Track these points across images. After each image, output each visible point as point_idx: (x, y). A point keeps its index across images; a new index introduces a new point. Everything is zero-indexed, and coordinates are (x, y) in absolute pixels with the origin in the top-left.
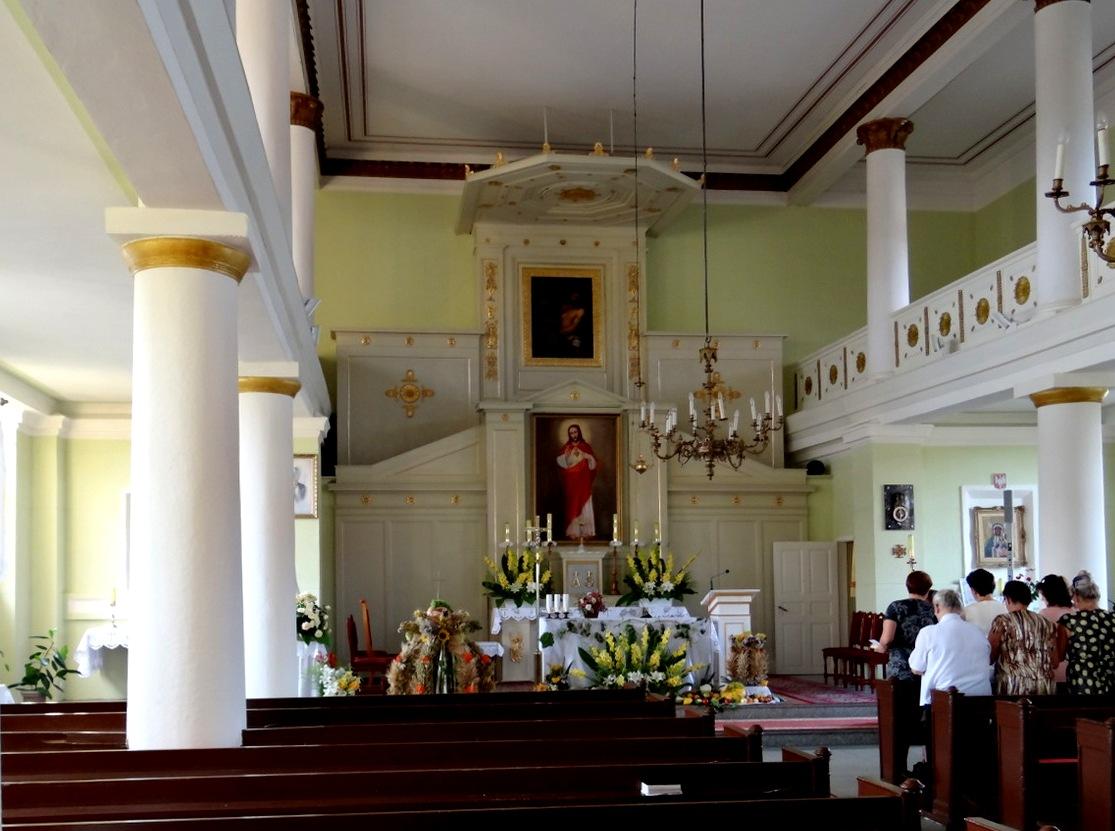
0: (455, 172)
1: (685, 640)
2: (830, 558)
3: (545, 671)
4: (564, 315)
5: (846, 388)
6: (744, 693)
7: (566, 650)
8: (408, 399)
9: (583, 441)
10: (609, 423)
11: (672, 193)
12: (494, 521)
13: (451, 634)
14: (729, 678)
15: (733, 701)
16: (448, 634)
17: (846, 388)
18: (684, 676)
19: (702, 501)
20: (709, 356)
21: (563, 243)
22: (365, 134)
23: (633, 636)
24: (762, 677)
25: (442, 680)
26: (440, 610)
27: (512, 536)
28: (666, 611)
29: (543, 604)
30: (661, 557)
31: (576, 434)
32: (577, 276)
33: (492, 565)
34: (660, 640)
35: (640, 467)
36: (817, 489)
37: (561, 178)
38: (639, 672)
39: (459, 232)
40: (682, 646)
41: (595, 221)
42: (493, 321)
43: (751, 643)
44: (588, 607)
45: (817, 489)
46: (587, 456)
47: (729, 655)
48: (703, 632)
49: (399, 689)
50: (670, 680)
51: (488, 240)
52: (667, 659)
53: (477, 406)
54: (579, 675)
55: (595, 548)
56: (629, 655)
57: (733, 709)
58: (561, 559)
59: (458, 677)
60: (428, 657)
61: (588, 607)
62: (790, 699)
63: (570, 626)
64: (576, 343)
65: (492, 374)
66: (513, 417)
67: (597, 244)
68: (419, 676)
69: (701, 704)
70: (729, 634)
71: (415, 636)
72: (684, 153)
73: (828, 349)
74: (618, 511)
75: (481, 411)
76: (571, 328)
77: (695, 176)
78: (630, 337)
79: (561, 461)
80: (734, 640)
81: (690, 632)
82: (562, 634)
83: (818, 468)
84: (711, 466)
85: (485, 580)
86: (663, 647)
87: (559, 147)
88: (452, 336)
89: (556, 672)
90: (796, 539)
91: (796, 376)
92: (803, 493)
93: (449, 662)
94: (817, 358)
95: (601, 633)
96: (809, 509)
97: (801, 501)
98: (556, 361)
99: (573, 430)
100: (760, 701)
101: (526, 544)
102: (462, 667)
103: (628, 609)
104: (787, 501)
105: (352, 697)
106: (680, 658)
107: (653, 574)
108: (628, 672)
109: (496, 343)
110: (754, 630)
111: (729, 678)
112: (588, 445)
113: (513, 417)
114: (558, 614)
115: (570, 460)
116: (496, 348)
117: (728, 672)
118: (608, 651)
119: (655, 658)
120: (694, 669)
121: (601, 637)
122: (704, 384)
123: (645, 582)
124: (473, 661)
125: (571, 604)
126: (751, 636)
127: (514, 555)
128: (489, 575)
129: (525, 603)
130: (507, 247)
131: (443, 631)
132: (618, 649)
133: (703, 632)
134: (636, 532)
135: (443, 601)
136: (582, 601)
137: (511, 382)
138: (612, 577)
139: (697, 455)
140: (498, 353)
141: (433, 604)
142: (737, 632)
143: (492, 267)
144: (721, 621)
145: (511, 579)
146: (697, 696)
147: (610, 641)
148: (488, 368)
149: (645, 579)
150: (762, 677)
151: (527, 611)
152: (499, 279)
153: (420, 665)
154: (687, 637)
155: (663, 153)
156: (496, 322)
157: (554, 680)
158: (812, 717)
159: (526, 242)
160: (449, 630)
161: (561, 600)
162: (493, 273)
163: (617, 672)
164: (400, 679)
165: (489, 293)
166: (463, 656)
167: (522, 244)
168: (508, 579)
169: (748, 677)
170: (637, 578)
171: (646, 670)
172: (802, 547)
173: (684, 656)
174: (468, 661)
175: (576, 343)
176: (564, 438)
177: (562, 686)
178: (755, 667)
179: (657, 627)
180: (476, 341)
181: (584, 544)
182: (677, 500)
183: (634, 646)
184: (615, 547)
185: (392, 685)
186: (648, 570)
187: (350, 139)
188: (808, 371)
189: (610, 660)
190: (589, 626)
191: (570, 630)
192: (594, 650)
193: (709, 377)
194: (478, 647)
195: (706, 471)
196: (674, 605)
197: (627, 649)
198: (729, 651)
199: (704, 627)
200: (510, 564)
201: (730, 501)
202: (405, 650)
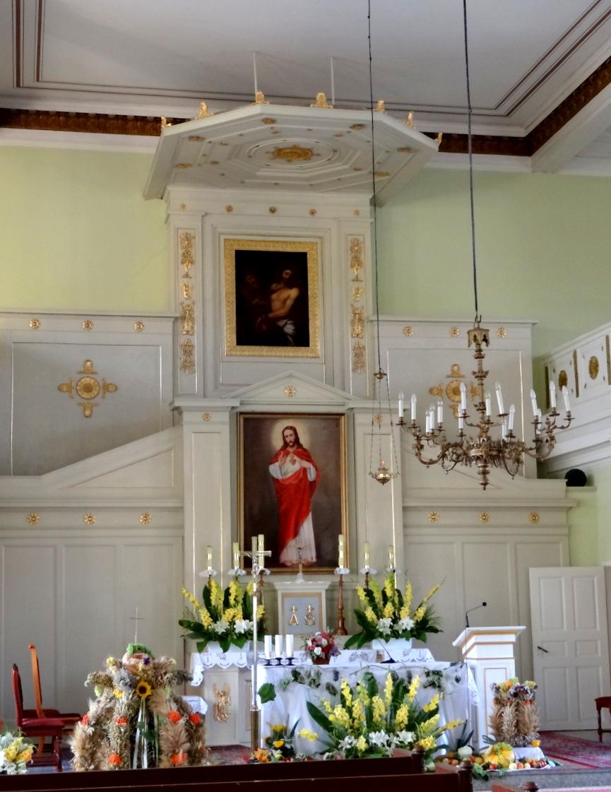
0: (149, 126)
1: (437, 689)
2: (595, 583)
3: (265, 732)
4: (274, 296)
5: (577, 395)
6: (513, 756)
7: (291, 706)
8: (85, 395)
9: (300, 446)
10: (332, 422)
11: (404, 154)
12: (193, 544)
13: (153, 688)
14: (493, 737)
15: (500, 766)
16: (149, 688)
17: (577, 395)
18: (438, 736)
19: (444, 518)
20: (480, 338)
21: (273, 211)
22: (38, 80)
23: (373, 689)
24: (532, 736)
25: (141, 748)
26: (139, 657)
27: (215, 564)
28: (405, 655)
29: (261, 648)
30: (396, 587)
31: (292, 438)
32: (289, 249)
33: (192, 599)
34: (407, 691)
35: (381, 476)
36: (579, 503)
37: (276, 133)
39: (148, 197)
40: (434, 699)
41: (311, 185)
42: (189, 302)
43: (519, 693)
44: (318, 651)
45: (579, 503)
46: (306, 464)
47: (491, 709)
48: (458, 680)
49: (86, 760)
51: (183, 206)
52: (416, 714)
53: (172, 403)
54: (308, 738)
55: (317, 577)
56: (369, 711)
57: (500, 777)
58: (275, 591)
59: (162, 742)
60: (125, 719)
61: (318, 651)
62: (568, 763)
63: (296, 675)
64: (289, 329)
65: (188, 365)
66: (215, 417)
67: (313, 213)
68: (113, 743)
70: (490, 681)
71: (106, 690)
72: (423, 111)
73: (588, 337)
74: (344, 530)
75: (177, 409)
76: (283, 312)
77: (433, 136)
78: (353, 322)
79: (275, 470)
80: (498, 689)
81: (443, 681)
82: (285, 685)
83: (577, 478)
84: (485, 473)
85: (181, 618)
86: (411, 700)
87: (273, 97)
88: (140, 319)
89: (279, 734)
90: (558, 565)
91: (546, 369)
92: (563, 508)
93: (151, 725)
94: (572, 348)
95: (336, 684)
96: (570, 527)
97: (561, 518)
98: (264, 350)
99: (288, 432)
100: (532, 766)
101: (232, 573)
102: (167, 730)
103: (359, 652)
104: (544, 518)
105: (310, 767)
106: (432, 713)
107: (389, 609)
108: (369, 732)
109: (193, 328)
111: (493, 737)
112: (305, 450)
113: (215, 417)
114: (279, 659)
115: (285, 469)
116: (192, 335)
118: (344, 706)
119: (402, 714)
120: (450, 727)
121: (333, 688)
122: (474, 373)
123: (378, 619)
124: (182, 721)
125: (295, 648)
126: (518, 684)
127: (218, 587)
128: (187, 611)
129: (232, 646)
130: (206, 214)
131: (142, 684)
132: (356, 703)
133: (458, 680)
134: (367, 556)
135: (142, 645)
136: (310, 643)
137: (210, 372)
138: (337, 615)
139: (464, 458)
140: (196, 341)
141: (129, 649)
142: (501, 680)
143: (188, 238)
145: (215, 617)
147: (346, 693)
148: (184, 357)
149: (380, 615)
150: (532, 736)
151: (236, 656)
152: (196, 252)
153: (114, 728)
154: (439, 687)
155: (396, 109)
156: (194, 303)
157: (277, 744)
158: (597, 785)
159: (229, 209)
160: (150, 682)
161: (273, 642)
162: (190, 245)
163: (357, 733)
164: (88, 746)
165: (184, 269)
166: (169, 715)
167: (225, 212)
168: (211, 616)
169: (516, 735)
170: (370, 614)
171: (390, 730)
172: (564, 574)
174: (175, 721)
175: (289, 329)
176: (277, 443)
177: (287, 752)
178: (524, 724)
179: (402, 674)
180: (168, 326)
181: (303, 572)
182: (414, 518)
183: (375, 699)
184: (341, 575)
185: (77, 754)
186: (382, 603)
187: (18, 85)
188: (562, 363)
189: (346, 717)
190: (318, 674)
191: (296, 679)
192: (327, 704)
193: (480, 364)
194: (186, 704)
195: (480, 479)
196: (414, 647)
197: (367, 702)
199: (459, 674)
200: (213, 598)
201: (476, 518)
202: (94, 709)
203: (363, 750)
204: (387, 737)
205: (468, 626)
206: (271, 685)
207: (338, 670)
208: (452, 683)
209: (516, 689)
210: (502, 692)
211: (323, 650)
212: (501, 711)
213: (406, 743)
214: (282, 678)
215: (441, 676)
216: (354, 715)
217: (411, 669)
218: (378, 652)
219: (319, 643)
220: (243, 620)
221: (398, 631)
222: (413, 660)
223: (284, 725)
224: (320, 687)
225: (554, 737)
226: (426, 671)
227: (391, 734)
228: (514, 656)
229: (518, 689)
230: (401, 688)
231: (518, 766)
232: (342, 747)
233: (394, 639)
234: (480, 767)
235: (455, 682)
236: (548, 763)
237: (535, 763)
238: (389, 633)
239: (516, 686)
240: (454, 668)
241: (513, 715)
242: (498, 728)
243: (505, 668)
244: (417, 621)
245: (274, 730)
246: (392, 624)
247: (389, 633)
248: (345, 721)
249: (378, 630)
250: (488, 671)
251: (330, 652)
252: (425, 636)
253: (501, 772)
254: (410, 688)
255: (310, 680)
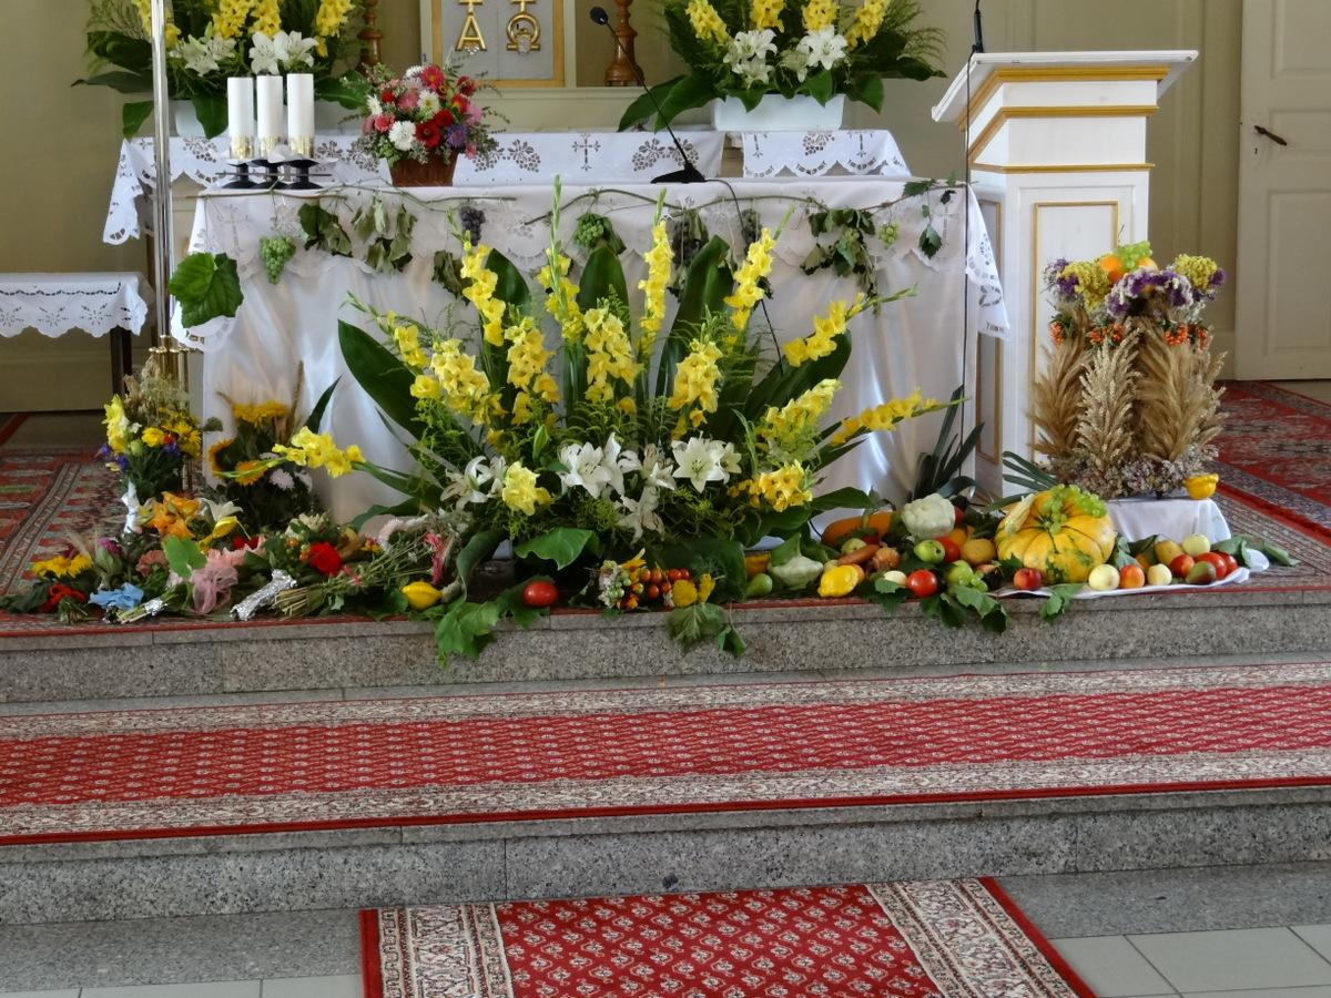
1: (853, 279)
6: (1107, 539)
15: (1055, 577)
24: (1193, 458)
34: (727, 283)
38: (614, 444)
43: (1149, 301)
47: (1048, 357)
48: (930, 246)
50: (762, 482)
61: (403, 135)
63: (318, 224)
69: (904, 593)
70: (1049, 254)
80: (1067, 285)
81: (873, 246)
82: (277, 260)
100: (1178, 573)
110: (1164, 238)
117: (1041, 433)
119: (699, 375)
126: (1150, 267)
132: (516, 332)
133: (930, 246)
144: (1017, 196)
146: (886, 553)
150: (1193, 458)
154: (860, 269)
173: (833, 364)
179: (721, 225)
189: (479, 385)
190: (405, 222)
196: (849, 123)
198: (1045, 335)
199: (938, 225)
203: (531, 512)
204: (632, 462)
205: (979, 48)
206: (222, 258)
207: (478, 206)
208: (909, 256)
209: (1138, 284)
210: (1087, 295)
211: (420, 134)
212: (1076, 367)
213: (700, 487)
214: (270, 235)
215: (870, 230)
216: (512, 377)
217: (759, 207)
218: (728, 139)
219: (409, 104)
220: (282, 34)
221: (792, 74)
222: (837, 169)
223: (286, 400)
224: (413, 265)
225: (1285, 411)
226: (814, 211)
227: (650, 450)
228: (1149, 158)
229: (1147, 288)
230: (711, 275)
231: (1122, 575)
232: (454, 500)
233: (780, 97)
234: (977, 579)
235: (919, 253)
236: (1241, 562)
237: (1189, 563)
238: (765, 78)
239: (1138, 274)
240: (916, 202)
241: (1119, 384)
242: (1060, 415)
243: (1114, 204)
244: (860, 40)
245: (240, 420)
246: (774, 48)
247: (765, 78)
248: (475, 404)
249: (728, 68)
250: (1042, 211)
251: (451, 139)
252: (881, 87)
253: (1053, 598)
254: (737, 276)
255: (371, 241)
